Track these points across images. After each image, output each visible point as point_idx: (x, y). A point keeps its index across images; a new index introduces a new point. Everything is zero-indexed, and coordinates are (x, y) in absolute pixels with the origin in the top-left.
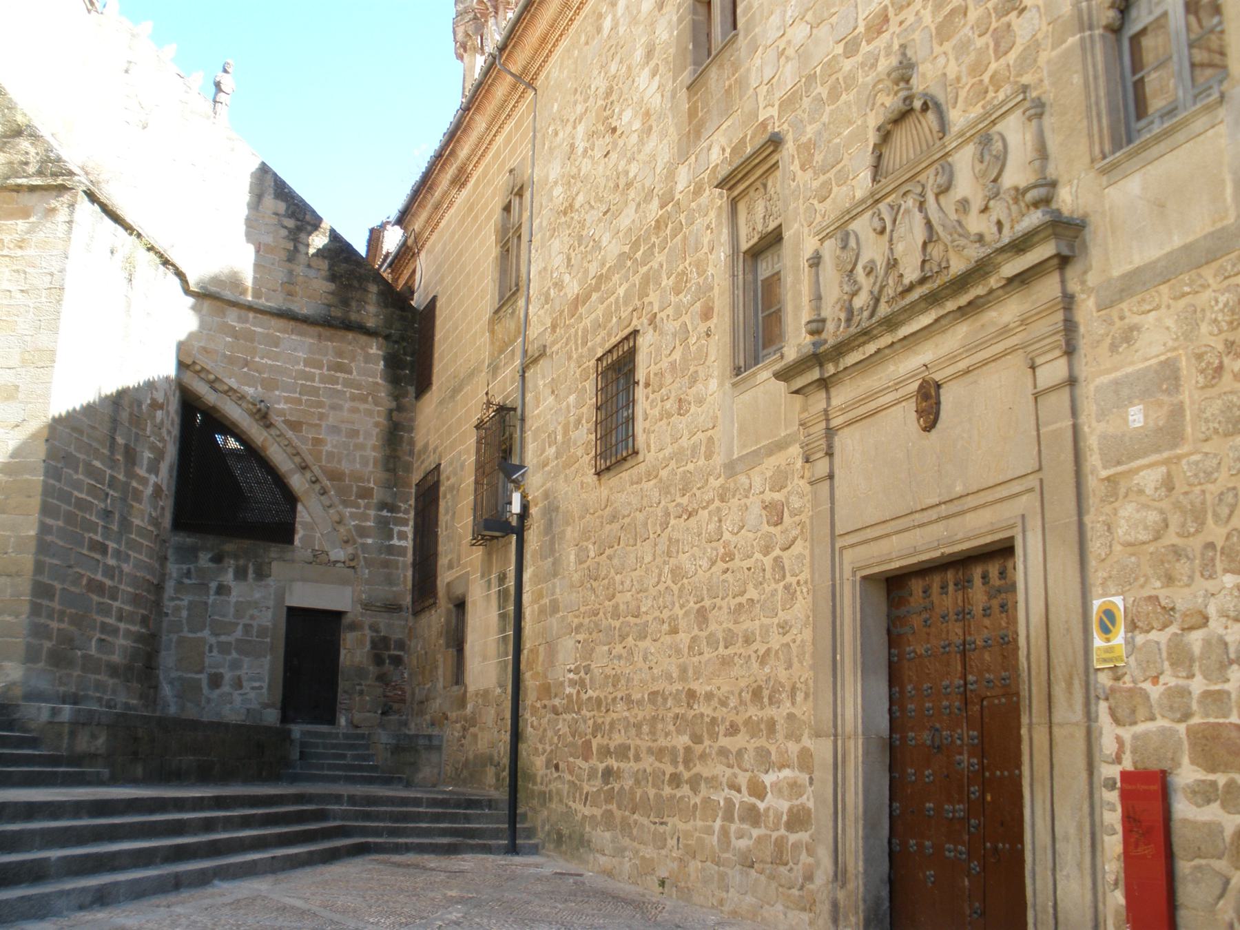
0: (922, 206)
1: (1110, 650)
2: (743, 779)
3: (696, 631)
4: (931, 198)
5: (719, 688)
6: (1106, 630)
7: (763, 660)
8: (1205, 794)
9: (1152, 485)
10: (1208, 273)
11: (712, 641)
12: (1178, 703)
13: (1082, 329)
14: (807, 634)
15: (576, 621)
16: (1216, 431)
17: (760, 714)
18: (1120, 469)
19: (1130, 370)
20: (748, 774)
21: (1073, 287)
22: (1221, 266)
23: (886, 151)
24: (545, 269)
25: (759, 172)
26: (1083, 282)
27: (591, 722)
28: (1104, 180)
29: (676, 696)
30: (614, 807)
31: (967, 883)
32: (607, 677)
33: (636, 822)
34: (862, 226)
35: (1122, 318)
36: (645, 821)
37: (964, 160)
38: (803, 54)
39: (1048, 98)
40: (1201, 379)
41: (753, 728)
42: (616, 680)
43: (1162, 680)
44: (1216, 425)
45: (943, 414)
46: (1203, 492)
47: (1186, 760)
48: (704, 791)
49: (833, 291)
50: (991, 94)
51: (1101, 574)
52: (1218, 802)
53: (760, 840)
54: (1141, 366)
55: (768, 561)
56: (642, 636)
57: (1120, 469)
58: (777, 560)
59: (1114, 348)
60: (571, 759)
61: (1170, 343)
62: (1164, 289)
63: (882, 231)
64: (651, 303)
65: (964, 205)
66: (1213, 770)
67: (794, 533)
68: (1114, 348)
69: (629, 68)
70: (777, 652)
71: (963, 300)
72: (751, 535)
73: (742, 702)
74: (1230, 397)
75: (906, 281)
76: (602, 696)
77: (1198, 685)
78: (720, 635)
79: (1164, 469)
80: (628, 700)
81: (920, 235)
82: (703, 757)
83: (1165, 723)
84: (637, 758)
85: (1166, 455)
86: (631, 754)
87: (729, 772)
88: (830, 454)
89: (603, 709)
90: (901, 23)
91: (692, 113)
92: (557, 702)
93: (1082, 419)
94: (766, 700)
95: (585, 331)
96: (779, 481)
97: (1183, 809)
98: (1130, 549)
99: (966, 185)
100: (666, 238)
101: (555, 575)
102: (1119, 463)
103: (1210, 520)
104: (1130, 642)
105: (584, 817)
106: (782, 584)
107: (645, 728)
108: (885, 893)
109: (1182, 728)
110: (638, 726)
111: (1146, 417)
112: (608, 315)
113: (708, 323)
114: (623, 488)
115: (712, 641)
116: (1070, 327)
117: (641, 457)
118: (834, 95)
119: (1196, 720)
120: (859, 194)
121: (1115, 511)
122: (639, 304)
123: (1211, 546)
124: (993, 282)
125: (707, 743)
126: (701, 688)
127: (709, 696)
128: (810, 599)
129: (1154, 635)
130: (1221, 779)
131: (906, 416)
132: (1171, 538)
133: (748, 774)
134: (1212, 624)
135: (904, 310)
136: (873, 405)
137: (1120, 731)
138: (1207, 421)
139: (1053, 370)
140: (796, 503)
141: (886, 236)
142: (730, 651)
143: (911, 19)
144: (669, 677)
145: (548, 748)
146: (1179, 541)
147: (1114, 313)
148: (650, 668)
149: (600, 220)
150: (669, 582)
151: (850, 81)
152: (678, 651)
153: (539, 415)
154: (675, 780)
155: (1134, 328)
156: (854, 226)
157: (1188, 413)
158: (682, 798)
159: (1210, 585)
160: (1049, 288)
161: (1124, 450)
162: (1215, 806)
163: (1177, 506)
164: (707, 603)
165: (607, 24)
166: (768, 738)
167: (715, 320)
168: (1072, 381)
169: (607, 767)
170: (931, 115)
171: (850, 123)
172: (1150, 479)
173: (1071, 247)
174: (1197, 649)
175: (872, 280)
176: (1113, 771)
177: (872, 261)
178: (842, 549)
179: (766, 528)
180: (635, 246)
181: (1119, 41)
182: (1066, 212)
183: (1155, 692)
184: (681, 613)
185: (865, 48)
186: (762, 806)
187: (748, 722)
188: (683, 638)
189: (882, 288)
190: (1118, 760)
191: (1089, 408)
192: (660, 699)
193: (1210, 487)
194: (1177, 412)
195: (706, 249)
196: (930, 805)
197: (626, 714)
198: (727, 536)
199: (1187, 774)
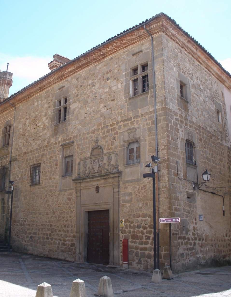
0: (98, 162)
1: (122, 225)
2: (62, 239)
3: (52, 215)
4: (100, 161)
5: (57, 224)
6: (121, 223)
7: (66, 221)
8: (132, 242)
10: (136, 183)
11: (56, 217)
12: (130, 232)
13: (120, 185)
14: (75, 218)
15: (23, 210)
17: (66, 229)
19: (126, 192)
20: (63, 238)
21: (120, 180)
23: (93, 152)
24: (17, 144)
25: (69, 146)
26: (121, 180)
27: (27, 228)
28: (125, 168)
29: (48, 225)
30: (33, 243)
31: (100, 253)
32: (31, 220)
33: (38, 245)
34: (88, 161)
35: (126, 185)
36: (41, 245)
37: (105, 158)
38: (79, 130)
39: (119, 154)
41: (64, 231)
42: (33, 221)
45: (99, 191)
47: (130, 238)
48: (53, 240)
49: (82, 169)
50: (110, 150)
51: (121, 216)
53: (65, 248)
55: (68, 206)
56: (40, 214)
58: (69, 206)
59: (124, 189)
60: (22, 234)
62: (131, 183)
63: (92, 163)
64: (44, 159)
65: (105, 164)
66: (133, 239)
67: (73, 203)
68: (124, 189)
69: (41, 115)
70: (69, 220)
71: (104, 178)
72: (64, 202)
73: (62, 227)
75: (95, 172)
76: (30, 224)
77: (132, 230)
78: (58, 216)
80: (37, 225)
81: (98, 166)
82: (54, 235)
83: (128, 234)
84: (38, 235)
86: (37, 234)
87: (59, 238)
88: (80, 193)
89: (30, 226)
91: (55, 130)
92: (18, 224)
93: (120, 196)
94: (67, 227)
95: (27, 159)
96: (70, 194)
97: (130, 243)
99: (105, 161)
100: (48, 149)
101: (18, 201)
102: (124, 203)
103: (135, 211)
104: (124, 224)
105: (25, 245)
106: (70, 210)
107: (40, 230)
108: (87, 255)
109: (130, 235)
110: (39, 229)
112: (33, 158)
113: (57, 166)
114: (36, 189)
115: (56, 217)
116: (119, 185)
117: (41, 185)
118: (84, 139)
120: (88, 156)
121: (123, 208)
122: (41, 158)
123: (134, 214)
124: (109, 176)
125: (54, 233)
126: (53, 224)
127: (55, 226)
128: (76, 213)
129: (127, 224)
130: (134, 240)
131: (94, 190)
132: (130, 213)
133: (63, 238)
136: (88, 187)
139: (116, 190)
140: (73, 198)
141: (92, 164)
142: (59, 219)
143: (98, 134)
144: (46, 222)
145: (15, 232)
146: (131, 213)
147: (125, 184)
148: (42, 220)
149: (32, 140)
150: (47, 206)
151: (87, 138)
152: (48, 218)
153: (14, 171)
154: (47, 238)
155: (127, 187)
156: (87, 160)
158: (49, 241)
159: (134, 219)
160: (116, 179)
161: (124, 201)
162: (133, 243)
163: (131, 209)
164: (55, 211)
165: (36, 104)
166: (67, 233)
167: (58, 166)
168: (119, 192)
169: (31, 236)
170: (101, 150)
171: (87, 145)
172: (128, 205)
173: (120, 175)
174: (132, 226)
175: (89, 170)
176: (122, 239)
177: (89, 167)
178: (82, 207)
179: (67, 201)
180: (41, 148)
181: (128, 149)
182: (120, 170)
183: (127, 230)
184: (49, 212)
185: (90, 134)
186: (66, 243)
187: (63, 230)
188: (50, 216)
189: (91, 171)
190: (122, 238)
191: (121, 196)
192: (44, 225)
193: (135, 208)
194: (132, 198)
195: (57, 154)
196: (94, 243)
197: (36, 227)
198: (59, 201)
199: (130, 240)
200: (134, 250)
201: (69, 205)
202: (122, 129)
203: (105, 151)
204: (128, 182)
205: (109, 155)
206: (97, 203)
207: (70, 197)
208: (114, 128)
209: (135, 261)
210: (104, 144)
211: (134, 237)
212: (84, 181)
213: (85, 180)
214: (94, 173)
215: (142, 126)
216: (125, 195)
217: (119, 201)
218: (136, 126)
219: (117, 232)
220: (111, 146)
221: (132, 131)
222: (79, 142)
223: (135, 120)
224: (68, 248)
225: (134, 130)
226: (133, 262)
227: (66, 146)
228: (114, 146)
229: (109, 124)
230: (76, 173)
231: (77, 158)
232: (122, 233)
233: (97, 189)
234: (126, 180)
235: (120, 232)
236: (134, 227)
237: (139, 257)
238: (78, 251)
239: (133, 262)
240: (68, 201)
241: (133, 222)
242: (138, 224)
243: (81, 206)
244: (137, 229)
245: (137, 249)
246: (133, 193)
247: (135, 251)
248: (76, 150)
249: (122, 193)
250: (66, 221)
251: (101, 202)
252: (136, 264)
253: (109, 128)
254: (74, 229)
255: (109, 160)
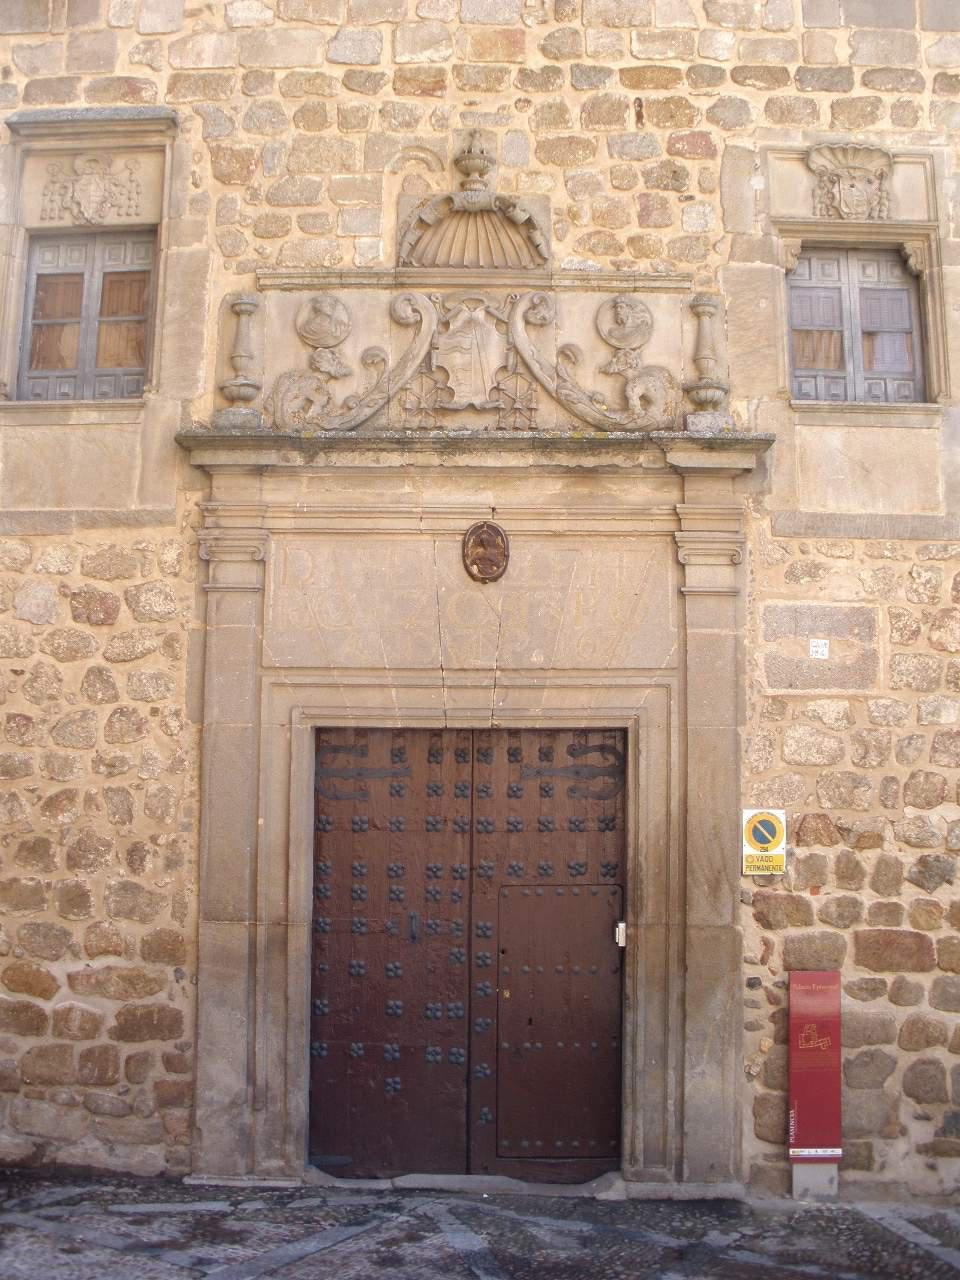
7: (52, 805)
8: (872, 990)
9: (834, 716)
16: (909, 685)
18: (791, 691)
22: (926, 547)
38: (251, 40)
40: (896, 636)
43: (823, 890)
44: (911, 680)
46: (889, 733)
50: (627, 255)
52: (886, 996)
54: (827, 603)
57: (791, 691)
61: (863, 594)
66: (881, 970)
72: (25, 627)
74: (927, 659)
79: (846, 704)
85: (851, 692)
90: (471, 104)
98: (795, 768)
104: (790, 854)
109: (847, 935)
111: (831, 651)
119: (863, 927)
130: (889, 978)
131: (448, 559)
134: (886, 845)
135: (346, 440)
136: (368, 524)
137: (769, 934)
138: (900, 673)
147: (795, 544)
155: (817, 567)
157: (881, 661)
161: (796, 675)
171: (346, 167)
172: (832, 709)
183: (816, 902)
186: (48, 1006)
194: (870, 657)
200: (891, 1049)
201: (97, 660)
202: (751, 127)
203: (564, 253)
204: (820, 526)
205: (622, 291)
206: (479, 664)
207: (103, 586)
208: (668, 100)
209: (904, 1132)
210: (560, 199)
211: (878, 951)
212: (321, 460)
213: (340, 459)
214: (443, 411)
215: (947, 150)
216: (800, 623)
217: (739, 668)
218: (884, 132)
219: (727, 919)
220: (635, 230)
221: (857, 163)
222: (242, 135)
223: (879, 100)
224: (87, 1056)
225: (876, 164)
226: (878, 1143)
227: (77, 135)
228: (666, 235)
229: (616, 66)
230: (773, 126)
231: (216, 259)
232: (764, 920)
233: (486, 552)
234: (807, 506)
235: (747, 913)
236: (888, 877)
237: (943, 1101)
238: (222, 1077)
239: (878, 1143)
240: (85, 628)
241: (877, 840)
242: (926, 852)
243: (266, 681)
244: (908, 895)
245: (930, 1042)
246: (882, 620)
247: (906, 1059)
248: (193, 191)
249: (767, 608)
250: (52, 805)
251: (537, 658)
252: (920, 1160)
253: (615, 88)
254: (182, 883)
255: (620, 331)
